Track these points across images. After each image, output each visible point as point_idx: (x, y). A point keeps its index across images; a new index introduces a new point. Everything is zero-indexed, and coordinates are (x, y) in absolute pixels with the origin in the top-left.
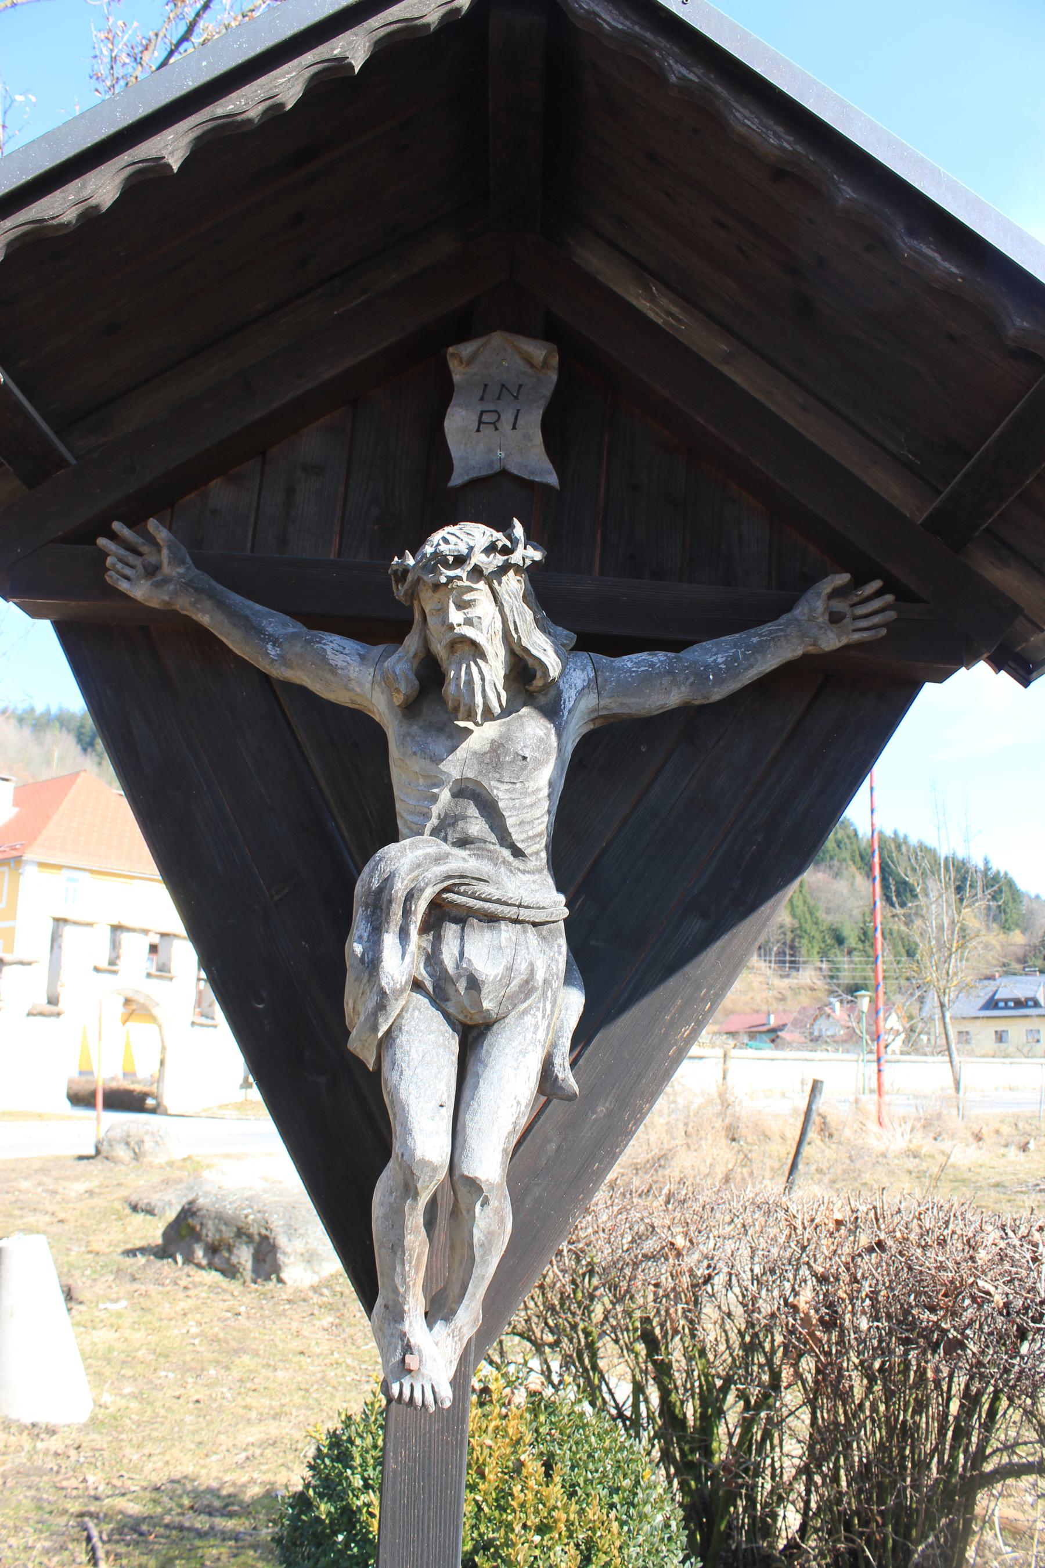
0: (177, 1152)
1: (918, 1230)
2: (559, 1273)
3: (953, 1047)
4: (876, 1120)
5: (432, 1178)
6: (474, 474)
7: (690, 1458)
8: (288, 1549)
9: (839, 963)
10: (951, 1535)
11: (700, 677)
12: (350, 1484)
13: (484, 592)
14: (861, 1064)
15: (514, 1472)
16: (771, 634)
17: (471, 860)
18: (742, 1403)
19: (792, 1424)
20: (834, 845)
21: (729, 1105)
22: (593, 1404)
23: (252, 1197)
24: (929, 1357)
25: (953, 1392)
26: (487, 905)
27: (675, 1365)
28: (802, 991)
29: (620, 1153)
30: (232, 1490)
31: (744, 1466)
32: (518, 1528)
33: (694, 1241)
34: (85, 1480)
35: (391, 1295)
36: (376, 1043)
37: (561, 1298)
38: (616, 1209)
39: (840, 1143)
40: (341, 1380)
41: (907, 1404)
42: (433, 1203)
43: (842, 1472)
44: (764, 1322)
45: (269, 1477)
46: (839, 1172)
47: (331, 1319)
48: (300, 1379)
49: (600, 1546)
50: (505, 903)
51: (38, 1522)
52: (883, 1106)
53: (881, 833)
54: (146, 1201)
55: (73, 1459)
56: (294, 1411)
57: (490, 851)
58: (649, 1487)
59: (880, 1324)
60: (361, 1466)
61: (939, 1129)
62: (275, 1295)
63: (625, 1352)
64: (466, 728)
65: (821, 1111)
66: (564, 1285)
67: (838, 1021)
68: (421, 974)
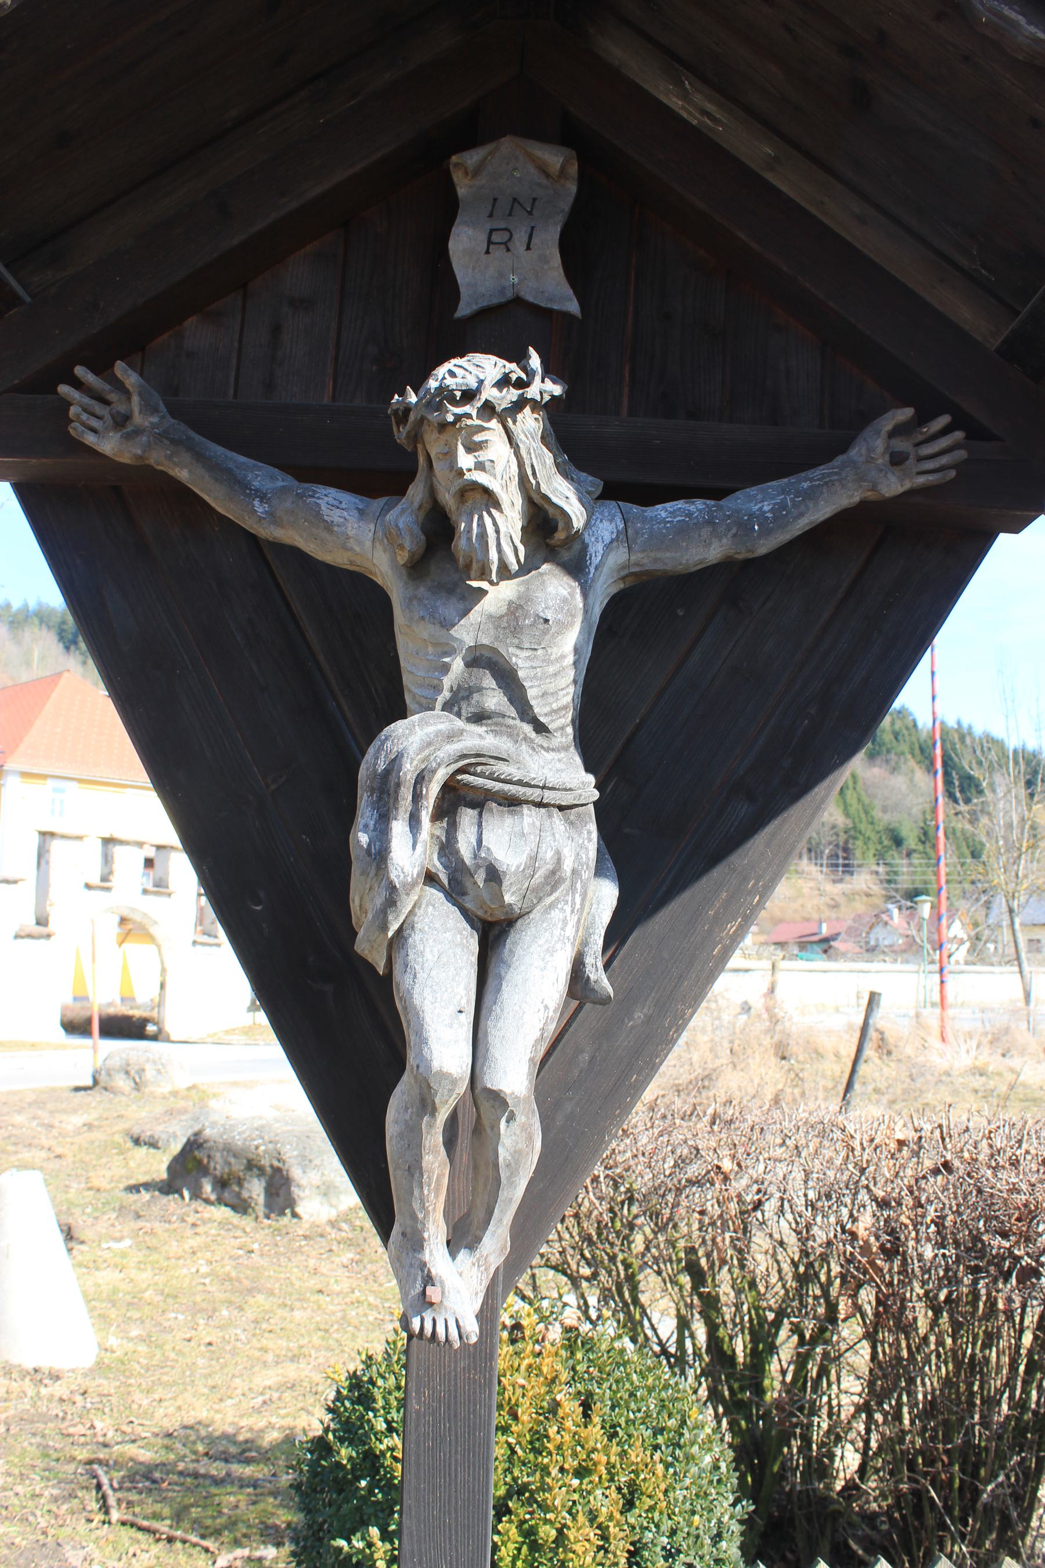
0: (182, 1082)
1: (987, 1151)
2: (595, 1201)
3: (1023, 955)
4: (939, 1035)
5: (451, 1091)
6: (484, 303)
7: (739, 1396)
8: (307, 1495)
9: (897, 865)
10: (1023, 1473)
11: (743, 527)
12: (372, 1428)
13: (497, 432)
14: (922, 975)
15: (549, 1413)
16: (824, 478)
17: (487, 737)
18: (795, 1338)
19: (850, 1360)
20: (891, 737)
21: (778, 1021)
22: (634, 1340)
23: (263, 1126)
24: (1001, 1286)
25: (1026, 1323)
26: (507, 787)
27: (723, 1299)
28: (857, 897)
29: (661, 1063)
30: (249, 1435)
31: (799, 1404)
32: (554, 1471)
33: (743, 1164)
34: (93, 1427)
35: (409, 1222)
36: (386, 943)
37: (598, 1228)
38: (656, 1131)
39: (899, 1061)
40: (364, 1319)
41: (975, 1337)
42: (453, 1120)
43: (905, 1410)
44: (819, 1251)
45: (288, 1422)
46: (899, 1092)
47: (350, 1255)
48: (319, 1319)
49: (644, 1489)
50: (527, 785)
51: (45, 1470)
52: (946, 1020)
53: (942, 723)
54: (148, 1133)
55: (79, 1404)
56: (313, 1352)
57: (509, 727)
58: (696, 1427)
59: (946, 1252)
60: (384, 1408)
61: (1007, 1045)
62: (290, 1230)
63: (669, 1285)
64: (480, 589)
65: (878, 1026)
66: (601, 1214)
67: (896, 929)
68: (434, 865)
